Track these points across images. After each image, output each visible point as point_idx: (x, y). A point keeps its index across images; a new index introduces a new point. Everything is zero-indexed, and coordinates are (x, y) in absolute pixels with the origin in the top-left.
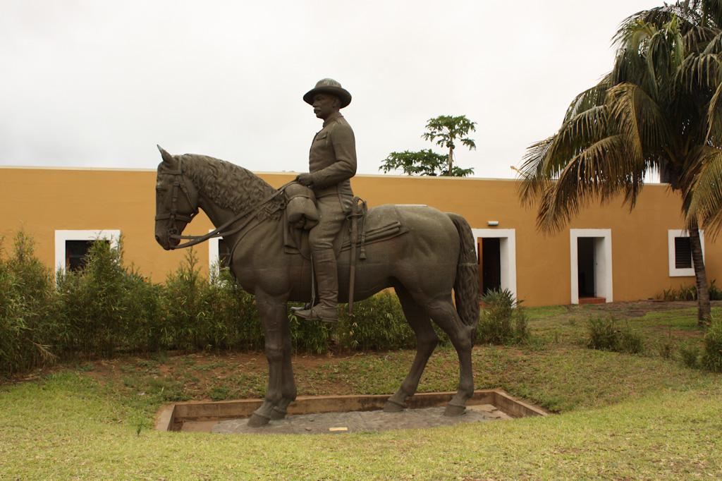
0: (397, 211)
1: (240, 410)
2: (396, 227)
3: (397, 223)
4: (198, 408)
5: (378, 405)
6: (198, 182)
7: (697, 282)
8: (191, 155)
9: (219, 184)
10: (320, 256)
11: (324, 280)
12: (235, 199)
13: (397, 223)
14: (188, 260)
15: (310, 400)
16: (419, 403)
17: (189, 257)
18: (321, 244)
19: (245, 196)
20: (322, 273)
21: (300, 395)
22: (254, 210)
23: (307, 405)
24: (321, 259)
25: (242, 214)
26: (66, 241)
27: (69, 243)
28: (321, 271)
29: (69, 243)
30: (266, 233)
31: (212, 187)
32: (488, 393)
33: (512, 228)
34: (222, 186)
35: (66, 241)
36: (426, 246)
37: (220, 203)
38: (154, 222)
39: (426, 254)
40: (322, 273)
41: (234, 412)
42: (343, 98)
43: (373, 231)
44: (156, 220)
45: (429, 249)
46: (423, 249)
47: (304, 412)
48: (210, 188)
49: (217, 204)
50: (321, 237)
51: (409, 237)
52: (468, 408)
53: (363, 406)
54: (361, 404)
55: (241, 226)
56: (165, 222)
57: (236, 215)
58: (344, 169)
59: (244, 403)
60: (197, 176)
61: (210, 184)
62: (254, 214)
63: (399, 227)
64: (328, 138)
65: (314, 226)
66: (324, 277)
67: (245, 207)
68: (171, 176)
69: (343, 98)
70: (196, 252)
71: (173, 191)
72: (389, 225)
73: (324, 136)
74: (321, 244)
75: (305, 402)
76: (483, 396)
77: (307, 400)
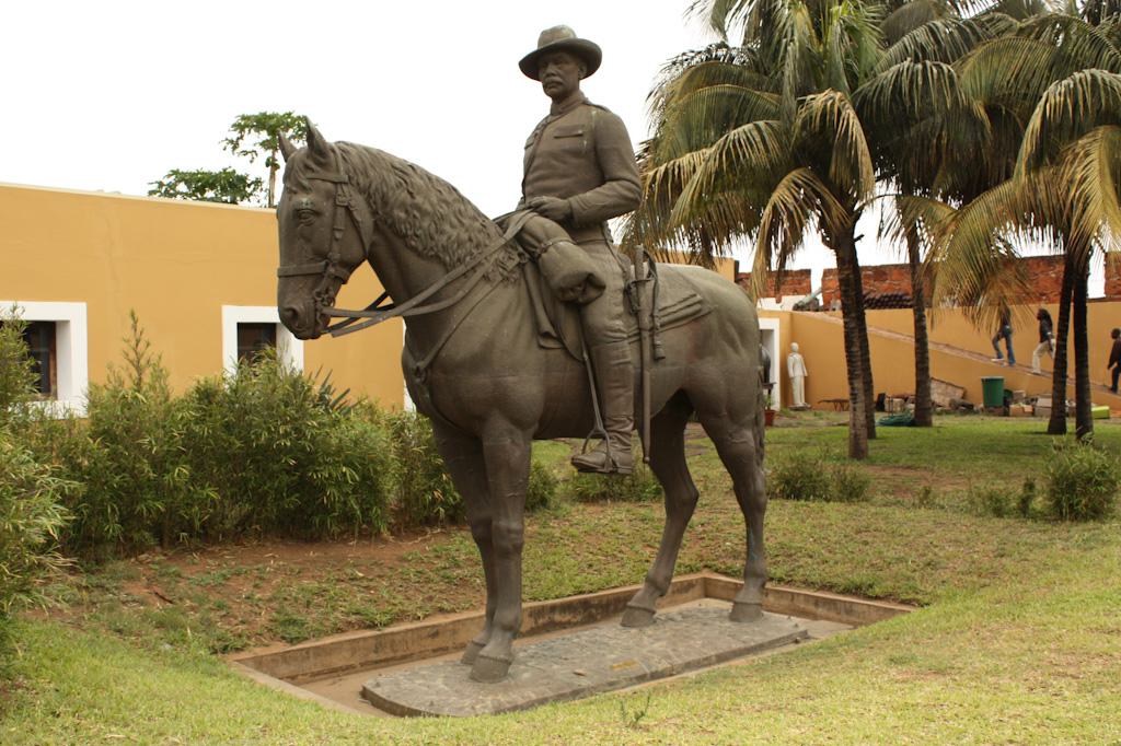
0: (679, 274)
1: (347, 655)
2: (695, 304)
3: (695, 295)
4: (273, 660)
5: (557, 617)
6: (379, 203)
7: (852, 394)
8: (321, 137)
9: (418, 208)
10: (615, 353)
11: (619, 396)
12: (449, 238)
13: (695, 295)
14: (131, 362)
15: (459, 621)
16: (612, 608)
17: (132, 356)
18: (616, 331)
19: (465, 236)
20: (617, 384)
21: (481, 617)
22: (480, 264)
23: (455, 632)
24: (618, 358)
25: (461, 269)
26: (238, 324)
27: (242, 327)
28: (617, 381)
29: (242, 327)
30: (508, 309)
31: (407, 212)
32: (697, 580)
33: (82, 301)
34: (424, 213)
35: (238, 324)
36: (736, 337)
37: (420, 248)
38: (277, 278)
39: (736, 350)
40: (617, 384)
41: (338, 661)
42: (587, 58)
43: (665, 308)
44: (280, 277)
45: (739, 343)
46: (732, 343)
47: (450, 644)
48: (402, 215)
49: (414, 249)
50: (613, 319)
51: (713, 321)
52: (661, 612)
53: (536, 622)
54: (533, 620)
55: (460, 294)
56: (310, 281)
57: (447, 271)
58: (631, 195)
59: (417, 629)
60: (377, 189)
61: (403, 206)
62: (480, 272)
63: (700, 302)
64: (587, 137)
65: (599, 296)
66: (621, 391)
67: (465, 256)
68: (329, 185)
69: (587, 58)
70: (148, 345)
71: (334, 215)
72: (685, 300)
73: (580, 132)
74: (616, 331)
75: (451, 626)
76: (690, 586)
77: (454, 622)
